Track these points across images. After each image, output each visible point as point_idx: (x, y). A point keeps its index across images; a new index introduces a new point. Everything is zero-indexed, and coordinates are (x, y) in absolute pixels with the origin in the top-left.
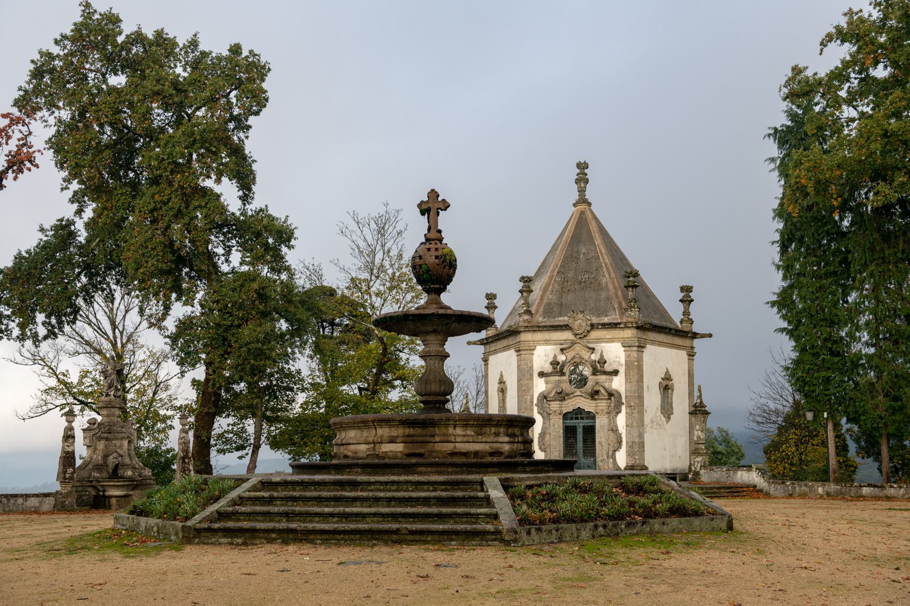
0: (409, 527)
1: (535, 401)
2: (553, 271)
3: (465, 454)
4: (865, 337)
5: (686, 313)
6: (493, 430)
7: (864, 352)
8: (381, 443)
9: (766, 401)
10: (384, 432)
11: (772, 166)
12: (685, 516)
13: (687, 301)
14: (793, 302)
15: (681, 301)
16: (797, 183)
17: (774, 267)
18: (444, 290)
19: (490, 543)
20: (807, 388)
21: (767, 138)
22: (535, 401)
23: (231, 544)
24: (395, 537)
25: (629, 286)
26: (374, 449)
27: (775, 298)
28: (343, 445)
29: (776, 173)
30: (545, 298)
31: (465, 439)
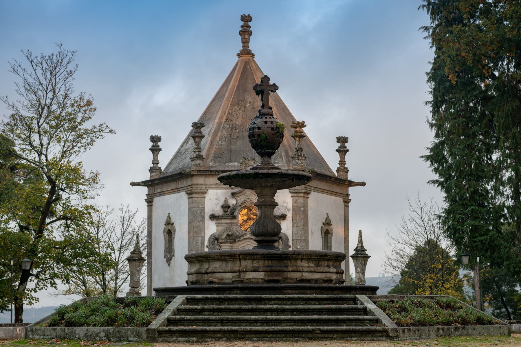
0: (321, 328)
1: (206, 243)
2: (221, 118)
3: (308, 281)
4: (508, 191)
5: (342, 162)
6: (326, 263)
7: (506, 204)
8: (246, 271)
9: (403, 246)
10: (247, 264)
11: (426, 34)
12: (484, 325)
13: (342, 151)
14: (444, 157)
15: (337, 151)
16: (457, 55)
17: (428, 125)
18: (273, 153)
19: (379, 338)
20: (457, 235)
21: (421, 9)
22: (206, 243)
23: (188, 342)
24: (310, 335)
25: (297, 136)
26: (239, 276)
27: (428, 153)
28: (207, 273)
29: (430, 40)
30: (215, 143)
31: (310, 269)
